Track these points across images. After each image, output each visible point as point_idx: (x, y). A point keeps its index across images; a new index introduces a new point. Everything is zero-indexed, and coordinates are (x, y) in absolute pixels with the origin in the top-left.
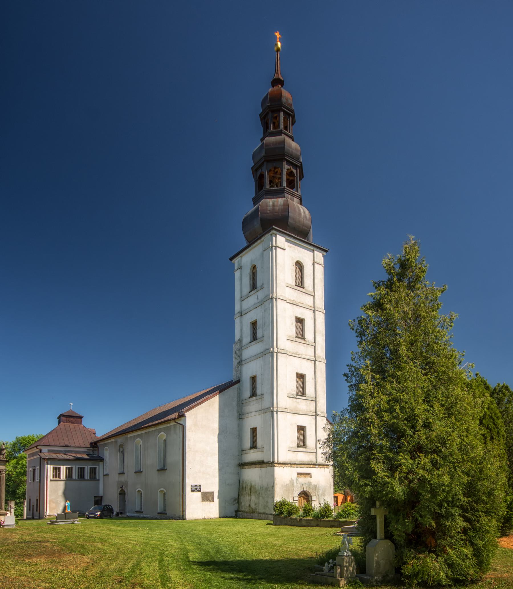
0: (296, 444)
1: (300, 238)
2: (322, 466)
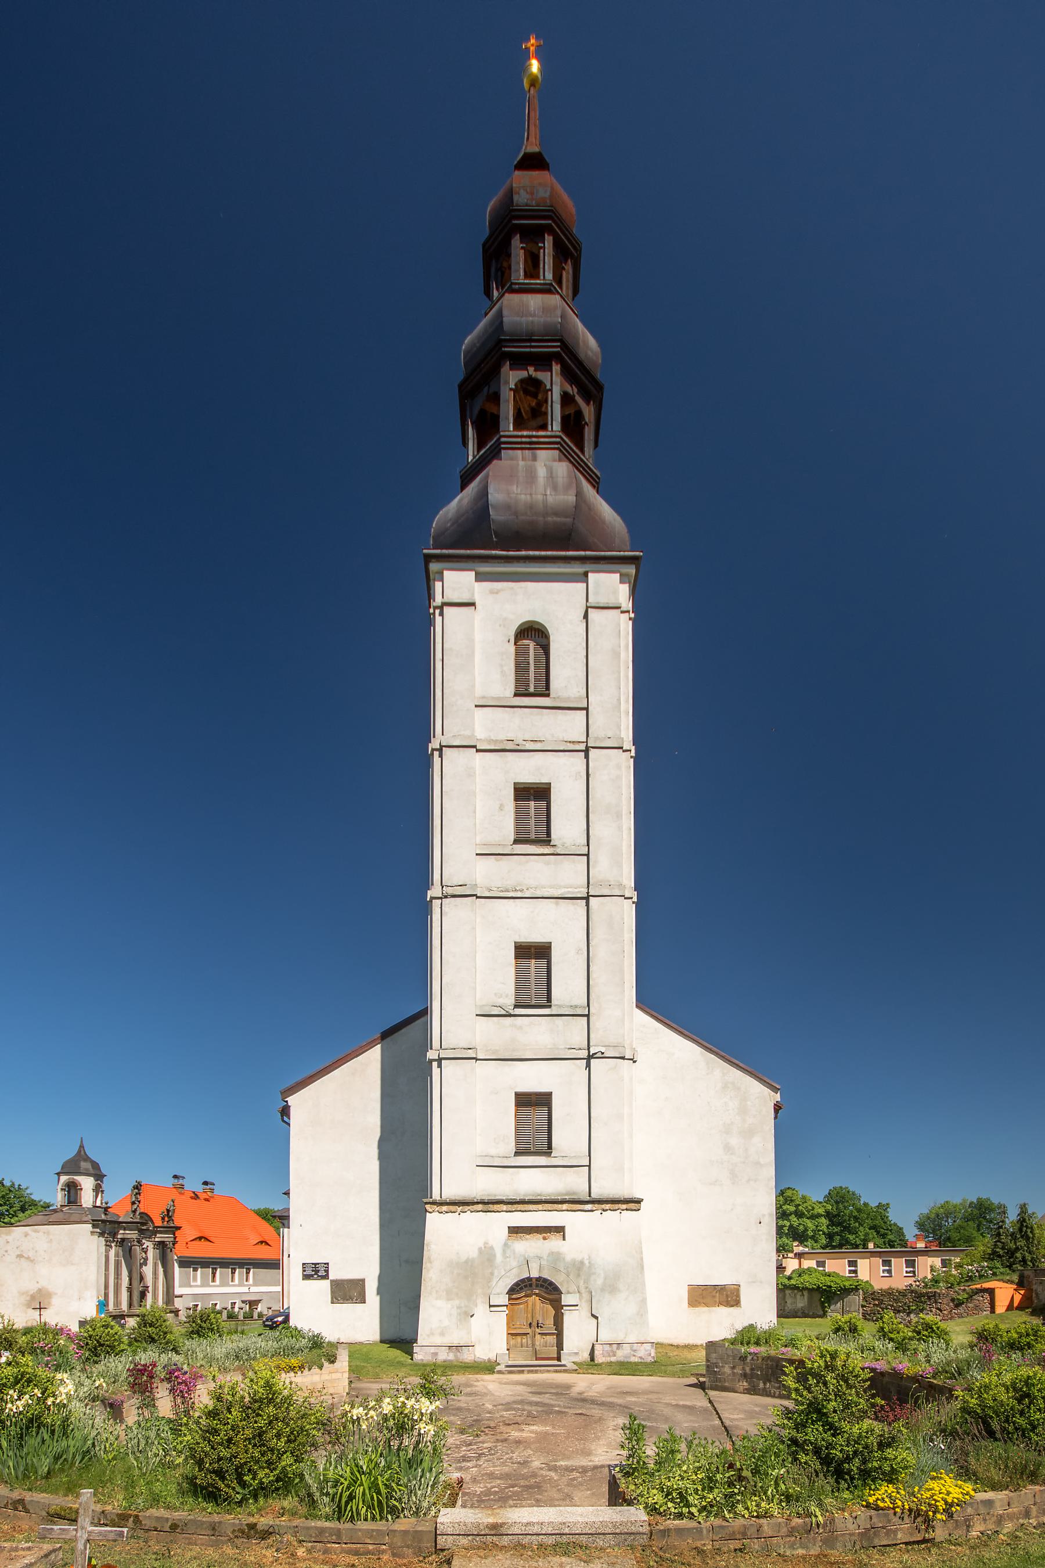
0: (512, 1147)
1: (523, 553)
2: (608, 1206)
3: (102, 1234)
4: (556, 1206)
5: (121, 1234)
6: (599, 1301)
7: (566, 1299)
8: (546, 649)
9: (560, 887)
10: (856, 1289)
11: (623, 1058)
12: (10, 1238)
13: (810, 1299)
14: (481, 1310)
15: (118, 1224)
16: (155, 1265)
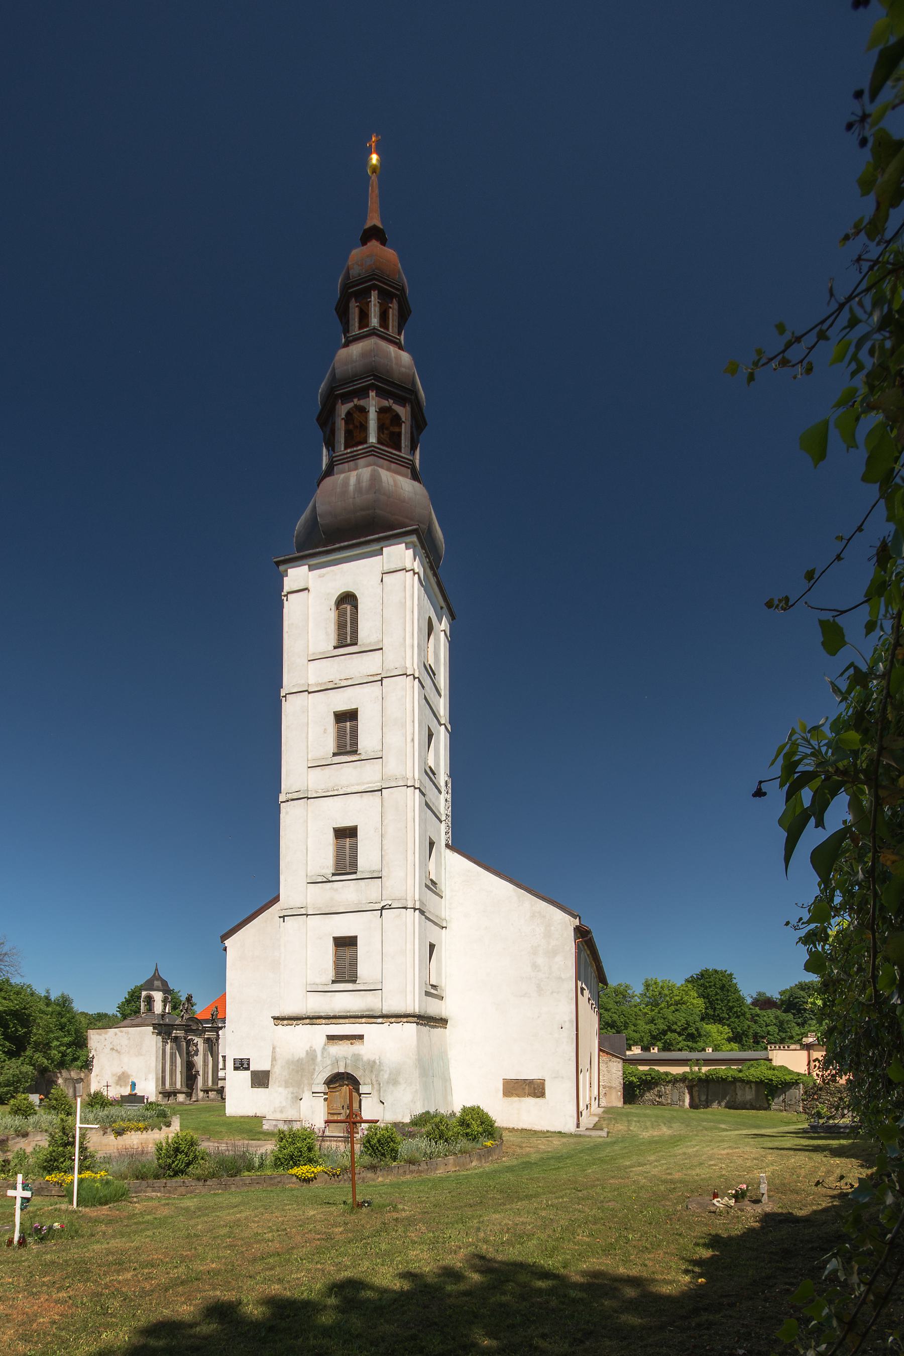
0: (330, 974)
1: (337, 546)
2: (393, 1020)
3: (159, 1034)
4: (357, 1020)
5: (175, 1033)
6: (385, 1091)
7: (363, 1089)
8: (356, 607)
9: (364, 784)
10: (796, 1083)
11: (406, 908)
12: (107, 1036)
13: (757, 1091)
14: (307, 1095)
15: (172, 1027)
16: (205, 1055)
